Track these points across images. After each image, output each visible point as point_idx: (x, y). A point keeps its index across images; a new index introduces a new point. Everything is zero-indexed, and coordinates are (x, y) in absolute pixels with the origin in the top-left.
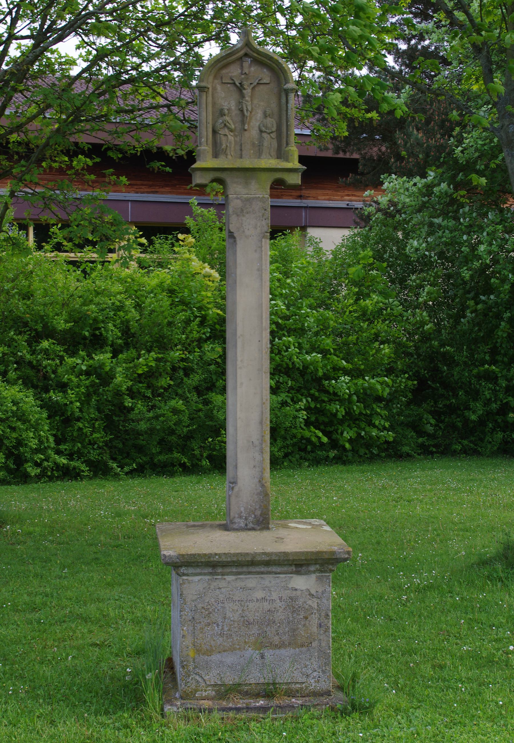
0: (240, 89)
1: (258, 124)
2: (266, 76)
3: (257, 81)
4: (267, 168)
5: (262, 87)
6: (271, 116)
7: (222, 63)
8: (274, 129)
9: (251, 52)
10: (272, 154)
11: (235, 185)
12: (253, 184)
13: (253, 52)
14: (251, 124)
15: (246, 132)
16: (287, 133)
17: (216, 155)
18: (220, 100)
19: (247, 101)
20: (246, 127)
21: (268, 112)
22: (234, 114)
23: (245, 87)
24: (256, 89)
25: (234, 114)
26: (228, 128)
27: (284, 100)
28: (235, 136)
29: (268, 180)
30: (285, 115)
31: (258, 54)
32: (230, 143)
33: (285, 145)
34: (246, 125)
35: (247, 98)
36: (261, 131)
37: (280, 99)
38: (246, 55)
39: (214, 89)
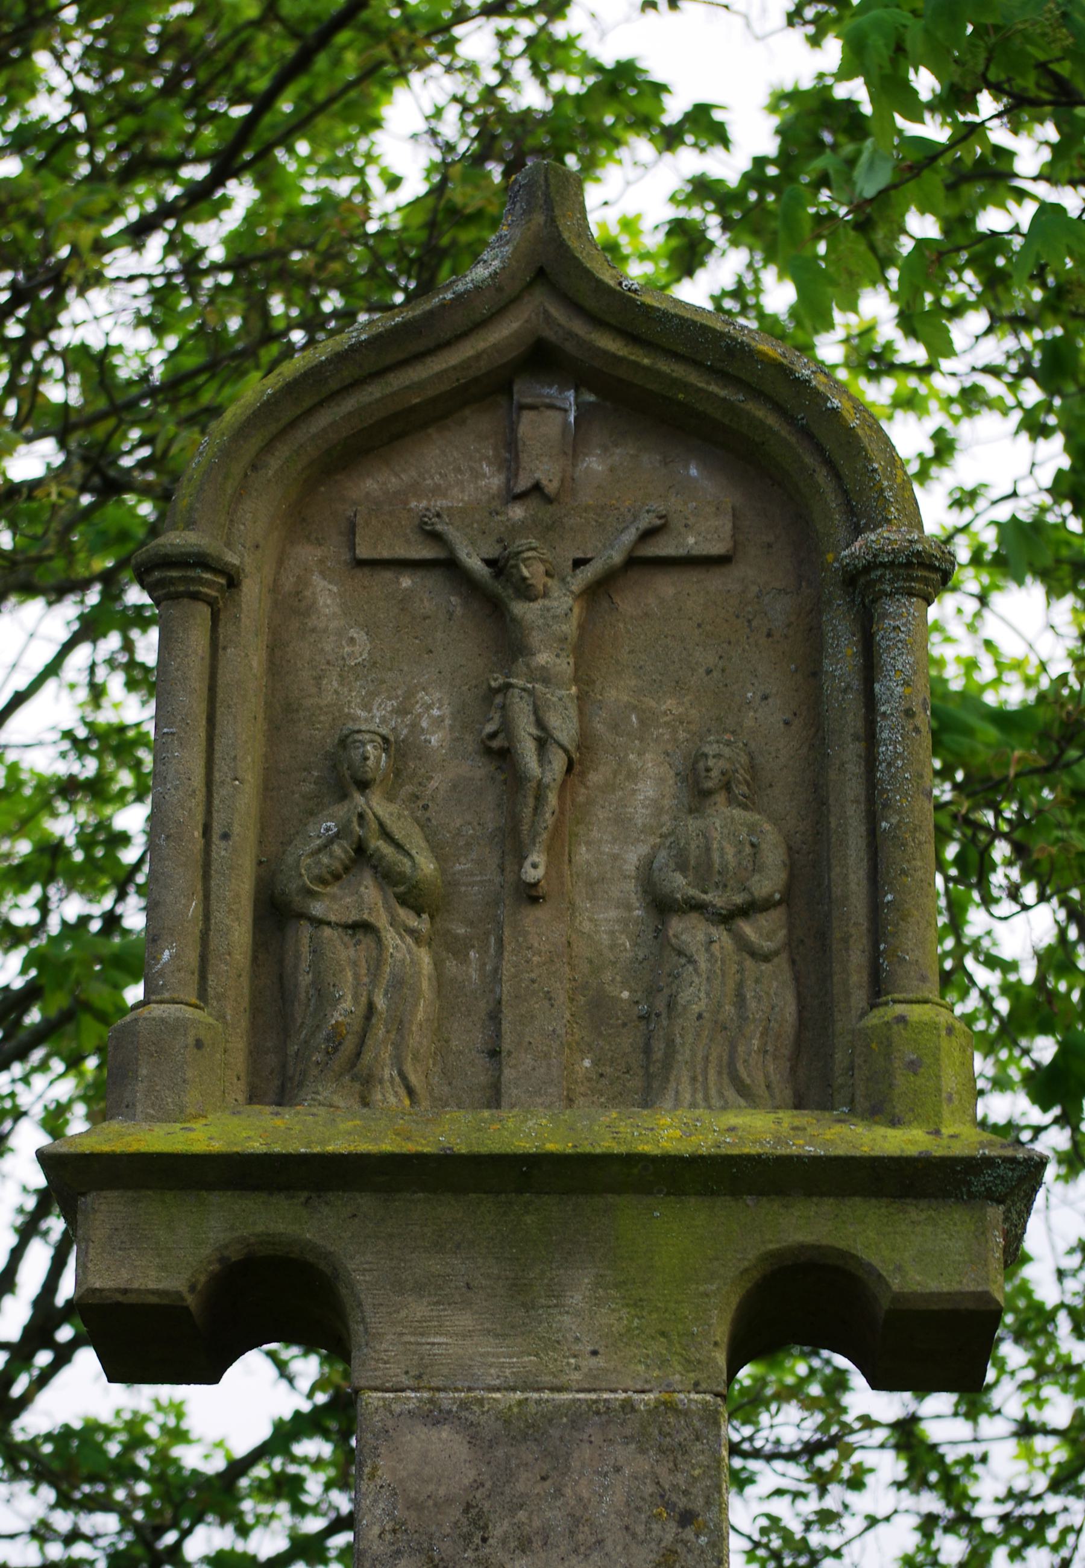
0: (491, 597)
1: (633, 857)
2: (701, 508)
3: (629, 537)
4: (695, 1161)
5: (667, 586)
6: (745, 787)
7: (349, 404)
8: (768, 883)
9: (579, 327)
10: (753, 1074)
11: (419, 1309)
12: (576, 1299)
13: (597, 321)
14: (583, 854)
15: (541, 913)
16: (876, 907)
17: (275, 1082)
18: (332, 683)
19: (545, 677)
20: (535, 868)
21: (720, 754)
22: (438, 782)
23: (532, 572)
24: (628, 602)
25: (438, 782)
26: (387, 877)
27: (842, 662)
28: (445, 946)
30: (855, 769)
31: (633, 338)
32: (398, 983)
33: (859, 997)
34: (537, 857)
35: (543, 658)
36: (662, 906)
37: (812, 671)
38: (541, 358)
39: (290, 607)
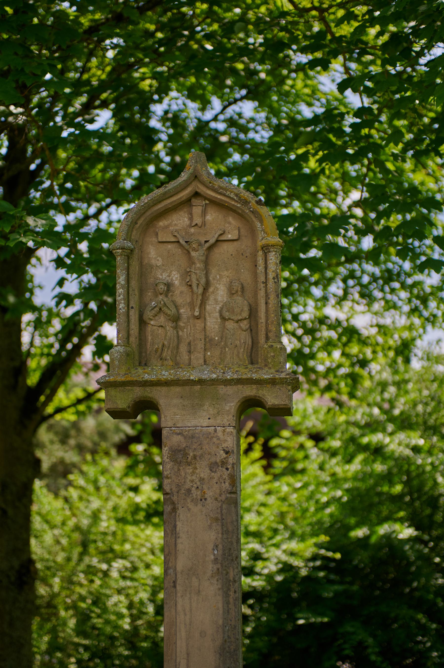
8: (245, 314)
27: (261, 261)
29: (232, 399)
38: (197, 194)
